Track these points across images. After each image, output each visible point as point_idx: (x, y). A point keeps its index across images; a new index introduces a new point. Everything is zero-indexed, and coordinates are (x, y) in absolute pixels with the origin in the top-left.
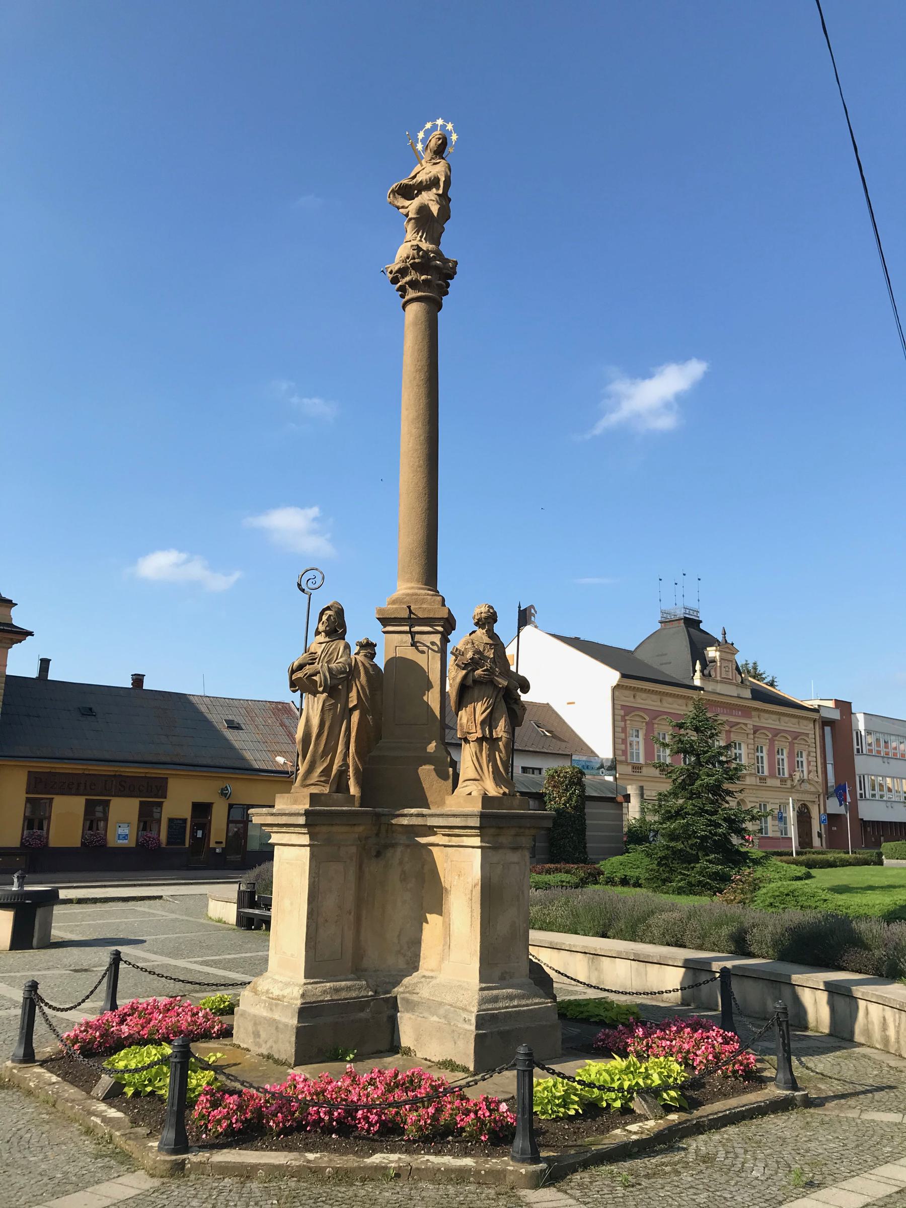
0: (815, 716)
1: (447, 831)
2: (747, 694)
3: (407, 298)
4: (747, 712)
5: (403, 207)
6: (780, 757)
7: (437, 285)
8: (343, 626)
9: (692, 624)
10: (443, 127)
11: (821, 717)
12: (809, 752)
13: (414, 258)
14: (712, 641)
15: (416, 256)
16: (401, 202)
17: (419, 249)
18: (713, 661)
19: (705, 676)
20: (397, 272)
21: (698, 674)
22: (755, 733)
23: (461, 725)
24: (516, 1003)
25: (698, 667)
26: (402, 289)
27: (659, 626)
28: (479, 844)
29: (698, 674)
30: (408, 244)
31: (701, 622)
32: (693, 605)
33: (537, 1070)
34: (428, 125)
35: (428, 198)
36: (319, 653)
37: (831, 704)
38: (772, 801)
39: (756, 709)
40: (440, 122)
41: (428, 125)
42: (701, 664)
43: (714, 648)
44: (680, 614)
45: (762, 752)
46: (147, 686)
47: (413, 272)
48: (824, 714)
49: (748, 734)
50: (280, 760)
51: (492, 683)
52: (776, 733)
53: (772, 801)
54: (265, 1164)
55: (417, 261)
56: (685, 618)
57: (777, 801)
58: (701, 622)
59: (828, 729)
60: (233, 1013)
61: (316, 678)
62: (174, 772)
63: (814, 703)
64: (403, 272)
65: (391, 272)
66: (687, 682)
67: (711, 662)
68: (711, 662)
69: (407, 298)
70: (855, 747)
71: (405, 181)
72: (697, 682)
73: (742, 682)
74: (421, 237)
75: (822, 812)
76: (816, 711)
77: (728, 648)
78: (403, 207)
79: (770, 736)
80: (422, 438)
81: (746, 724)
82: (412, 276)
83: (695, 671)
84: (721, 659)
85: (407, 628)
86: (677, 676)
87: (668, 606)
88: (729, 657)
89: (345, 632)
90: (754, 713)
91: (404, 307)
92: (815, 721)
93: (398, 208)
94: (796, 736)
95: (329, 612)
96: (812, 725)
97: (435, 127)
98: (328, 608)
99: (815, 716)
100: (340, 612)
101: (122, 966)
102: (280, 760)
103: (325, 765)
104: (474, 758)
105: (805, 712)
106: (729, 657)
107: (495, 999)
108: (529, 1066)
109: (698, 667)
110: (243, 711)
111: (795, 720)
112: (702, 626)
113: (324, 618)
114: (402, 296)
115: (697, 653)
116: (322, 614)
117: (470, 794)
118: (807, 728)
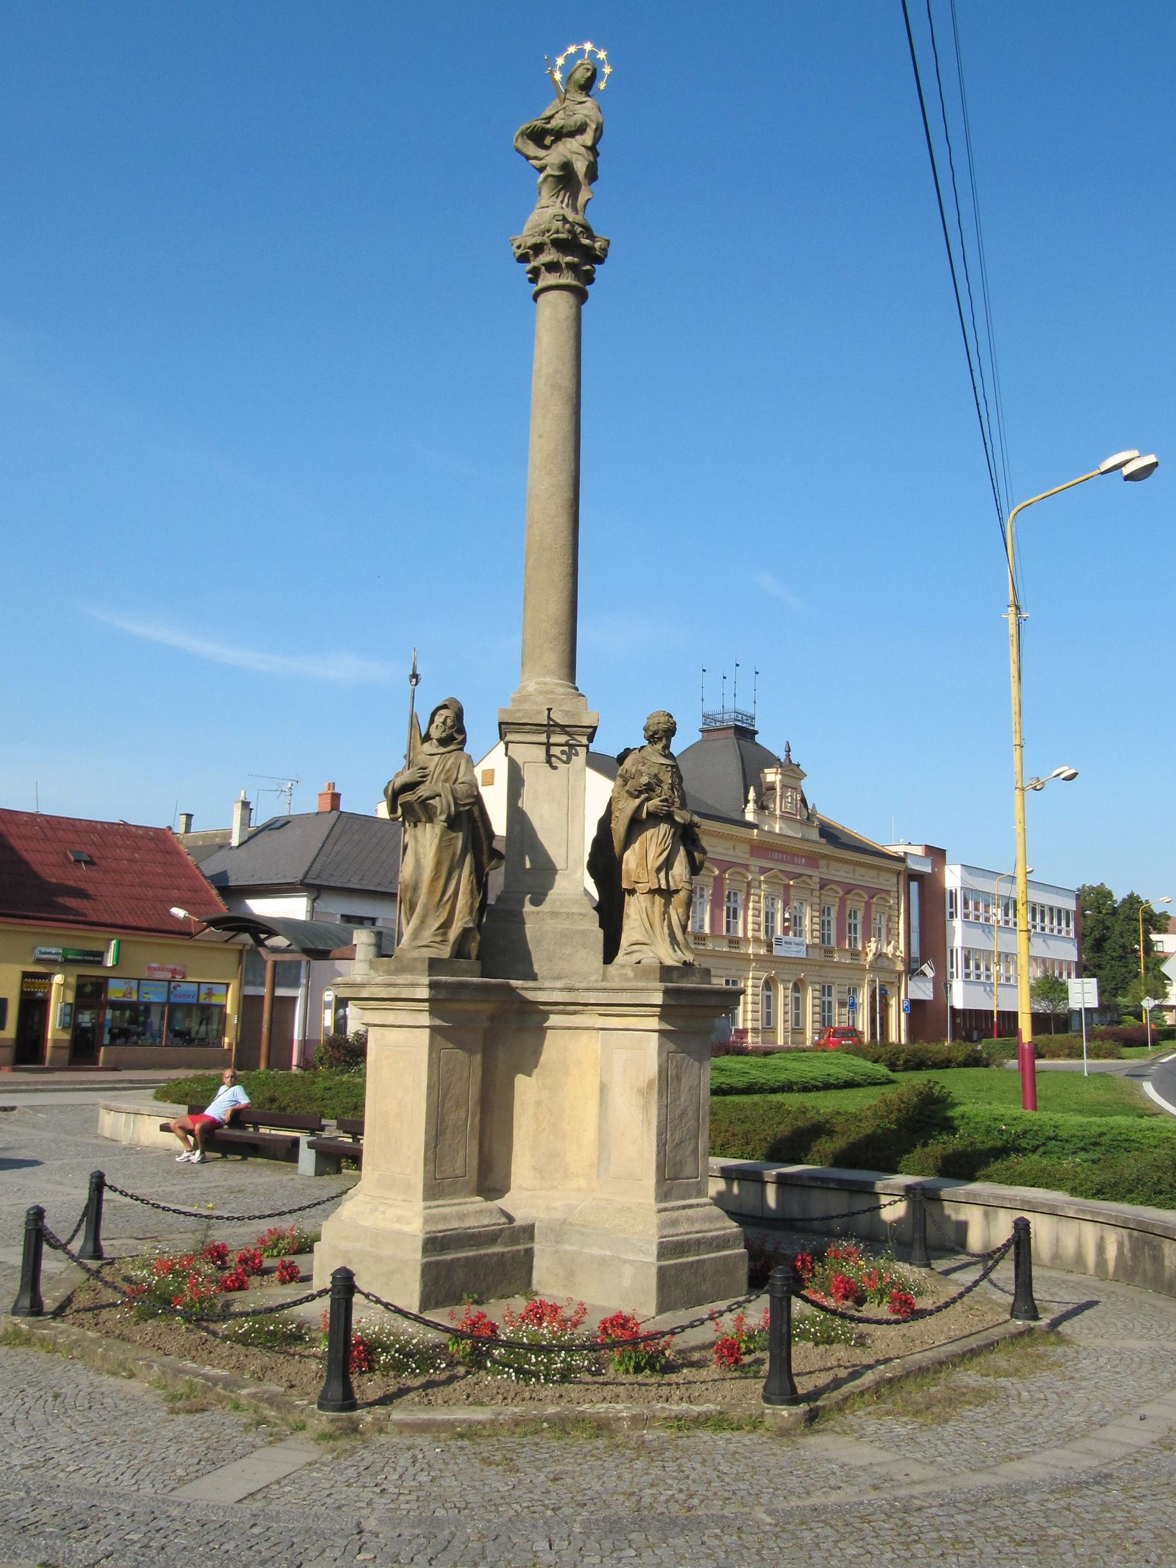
0: (899, 866)
1: (602, 1010)
2: (814, 835)
3: (542, 284)
4: (813, 860)
5: (536, 158)
6: (852, 921)
7: (567, 264)
8: (461, 730)
9: (744, 733)
10: (593, 54)
11: (907, 868)
12: (890, 917)
13: (557, 232)
14: (770, 760)
15: (561, 229)
16: (531, 149)
17: (565, 220)
18: (772, 788)
19: (761, 807)
20: (529, 248)
21: (751, 806)
22: (821, 888)
23: (628, 872)
24: (697, 1227)
25: (752, 795)
26: (535, 274)
27: (699, 736)
28: (657, 1027)
29: (751, 806)
30: (546, 212)
31: (756, 732)
32: (748, 709)
33: (794, 1299)
34: (572, 49)
35: (573, 150)
36: (431, 768)
37: (919, 851)
38: (839, 981)
39: (825, 856)
40: (588, 46)
41: (572, 49)
42: (756, 792)
43: (774, 770)
44: (729, 720)
45: (829, 915)
46: (344, 807)
47: (553, 250)
48: (912, 865)
49: (812, 890)
50: (179, 912)
51: (669, 818)
52: (849, 889)
53: (839, 981)
54: (464, 1421)
55: (561, 236)
56: (737, 728)
57: (846, 982)
58: (756, 732)
59: (914, 886)
60: (311, 1251)
61: (435, 802)
62: (59, 932)
63: (898, 850)
64: (538, 249)
65: (519, 247)
66: (735, 816)
67: (768, 789)
68: (768, 789)
69: (542, 284)
70: (948, 910)
71: (539, 123)
72: (750, 817)
73: (808, 818)
74: (562, 202)
75: (903, 997)
76: (901, 860)
77: (793, 772)
78: (536, 158)
79: (841, 893)
80: (561, 478)
81: (810, 877)
82: (545, 258)
83: (747, 801)
84: (784, 786)
85: (543, 738)
86: (724, 809)
87: (713, 707)
88: (793, 783)
89: (464, 742)
90: (822, 862)
91: (536, 297)
92: (899, 874)
93: (528, 158)
94: (873, 892)
95: (444, 712)
96: (894, 880)
97: (580, 53)
98: (445, 707)
99: (899, 866)
100: (459, 715)
101: (107, 1194)
102: (179, 912)
103: (441, 920)
104: (645, 916)
105: (888, 861)
106: (793, 783)
107: (674, 1223)
108: (788, 1292)
109: (752, 795)
110: (95, 838)
111: (873, 873)
112: (758, 739)
113: (439, 720)
114: (534, 281)
115: (750, 775)
116: (434, 714)
117: (639, 963)
118: (888, 882)
